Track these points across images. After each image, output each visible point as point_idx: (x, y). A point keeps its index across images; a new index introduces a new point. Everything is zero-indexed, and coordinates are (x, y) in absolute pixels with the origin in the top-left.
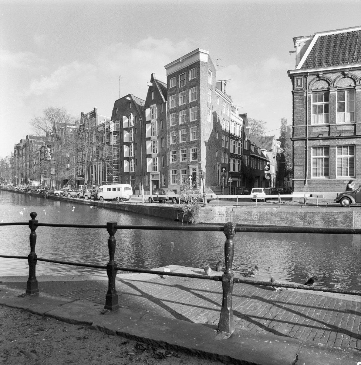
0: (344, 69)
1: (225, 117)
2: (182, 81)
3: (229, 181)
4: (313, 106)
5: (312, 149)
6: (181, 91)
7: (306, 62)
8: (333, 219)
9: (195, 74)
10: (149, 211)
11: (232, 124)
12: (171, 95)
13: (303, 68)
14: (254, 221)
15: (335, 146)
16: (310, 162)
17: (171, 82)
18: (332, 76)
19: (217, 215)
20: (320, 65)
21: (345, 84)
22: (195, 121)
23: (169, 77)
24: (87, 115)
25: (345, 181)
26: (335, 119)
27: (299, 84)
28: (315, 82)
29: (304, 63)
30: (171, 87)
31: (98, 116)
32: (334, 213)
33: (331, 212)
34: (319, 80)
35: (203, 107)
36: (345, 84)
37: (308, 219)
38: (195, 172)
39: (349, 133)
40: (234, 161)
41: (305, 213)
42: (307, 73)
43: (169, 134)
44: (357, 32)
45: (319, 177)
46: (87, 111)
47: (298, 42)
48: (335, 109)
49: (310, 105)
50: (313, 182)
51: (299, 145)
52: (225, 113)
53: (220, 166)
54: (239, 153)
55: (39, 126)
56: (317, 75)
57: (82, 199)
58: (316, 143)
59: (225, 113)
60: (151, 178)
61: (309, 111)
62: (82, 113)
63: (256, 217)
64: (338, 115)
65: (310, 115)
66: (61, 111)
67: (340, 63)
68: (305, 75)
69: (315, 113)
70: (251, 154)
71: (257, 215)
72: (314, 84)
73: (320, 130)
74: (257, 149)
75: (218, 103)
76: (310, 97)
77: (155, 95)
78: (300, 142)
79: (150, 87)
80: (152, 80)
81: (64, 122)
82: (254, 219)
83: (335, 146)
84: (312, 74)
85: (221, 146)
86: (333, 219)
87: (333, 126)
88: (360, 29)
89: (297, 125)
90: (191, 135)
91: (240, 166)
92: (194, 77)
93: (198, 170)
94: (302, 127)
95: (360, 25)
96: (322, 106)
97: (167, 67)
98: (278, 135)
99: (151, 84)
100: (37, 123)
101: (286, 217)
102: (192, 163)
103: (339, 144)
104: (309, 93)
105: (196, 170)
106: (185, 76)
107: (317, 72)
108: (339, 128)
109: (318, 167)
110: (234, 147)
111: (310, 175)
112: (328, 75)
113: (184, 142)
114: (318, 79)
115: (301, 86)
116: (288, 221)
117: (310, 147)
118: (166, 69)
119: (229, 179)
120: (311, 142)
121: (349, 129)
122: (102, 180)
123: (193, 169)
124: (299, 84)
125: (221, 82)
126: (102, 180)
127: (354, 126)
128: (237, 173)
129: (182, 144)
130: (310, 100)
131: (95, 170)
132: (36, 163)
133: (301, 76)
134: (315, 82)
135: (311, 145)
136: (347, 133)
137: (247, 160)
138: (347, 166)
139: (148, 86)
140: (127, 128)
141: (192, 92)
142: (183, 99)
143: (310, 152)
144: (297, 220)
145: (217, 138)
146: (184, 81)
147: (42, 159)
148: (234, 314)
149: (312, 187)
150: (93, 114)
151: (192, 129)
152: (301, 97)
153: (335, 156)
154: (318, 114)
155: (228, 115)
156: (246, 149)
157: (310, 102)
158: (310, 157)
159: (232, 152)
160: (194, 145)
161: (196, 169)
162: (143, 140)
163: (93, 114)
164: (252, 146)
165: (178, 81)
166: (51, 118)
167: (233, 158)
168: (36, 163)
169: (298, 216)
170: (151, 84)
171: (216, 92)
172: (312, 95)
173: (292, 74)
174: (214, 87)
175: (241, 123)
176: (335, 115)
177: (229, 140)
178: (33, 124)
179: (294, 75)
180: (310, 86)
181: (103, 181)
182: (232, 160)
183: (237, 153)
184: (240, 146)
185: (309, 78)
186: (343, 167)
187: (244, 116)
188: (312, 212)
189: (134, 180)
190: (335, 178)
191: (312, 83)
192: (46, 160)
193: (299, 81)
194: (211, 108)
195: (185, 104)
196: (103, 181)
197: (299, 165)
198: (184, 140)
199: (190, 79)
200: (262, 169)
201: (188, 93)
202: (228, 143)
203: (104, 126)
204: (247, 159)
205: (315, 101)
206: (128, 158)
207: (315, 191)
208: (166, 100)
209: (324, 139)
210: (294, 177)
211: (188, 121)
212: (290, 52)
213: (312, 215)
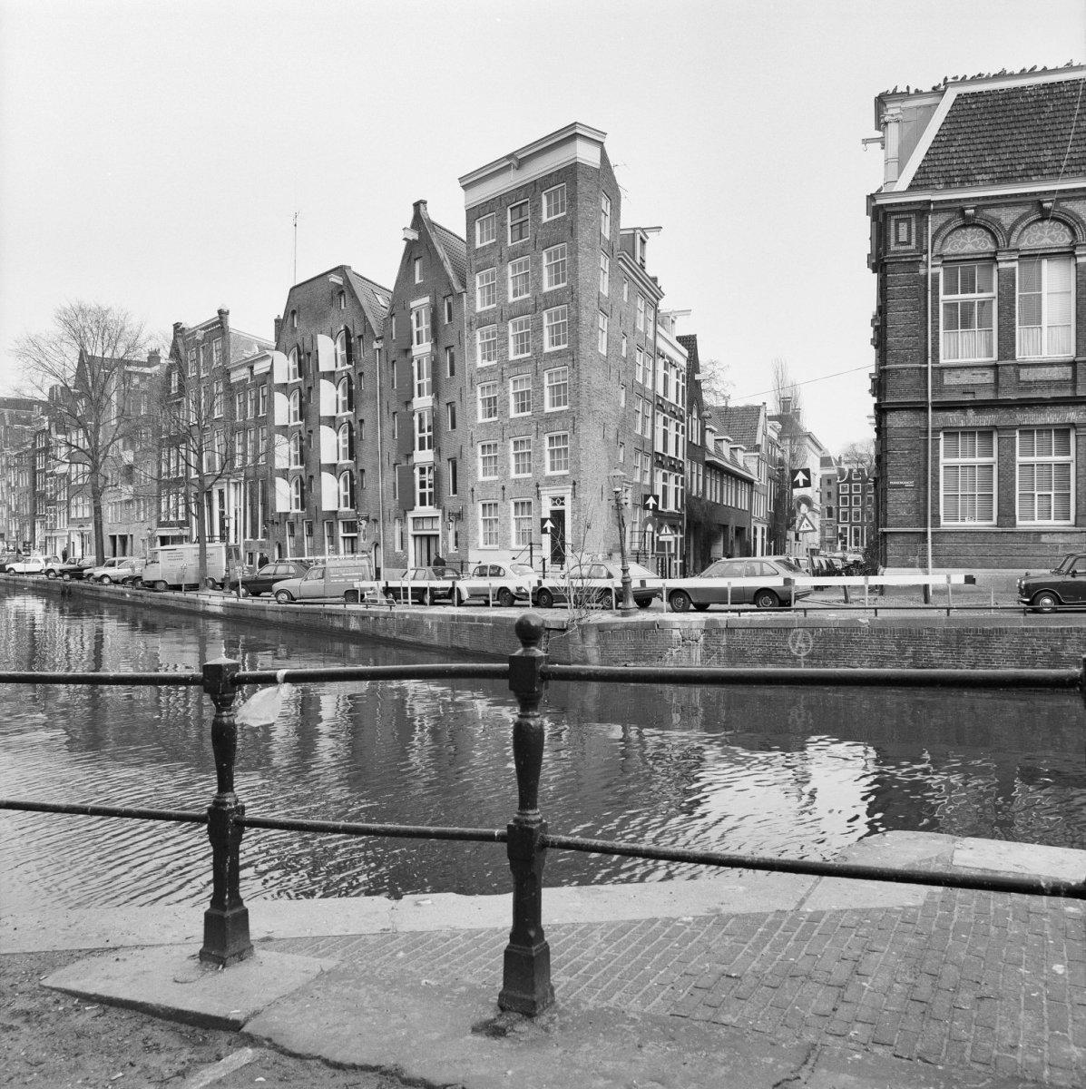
0: (1041, 193)
1: (642, 342)
2: (520, 228)
3: (661, 539)
4: (946, 305)
5: (942, 435)
6: (515, 254)
7: (921, 170)
8: (1049, 650)
9: (563, 203)
10: (435, 628)
11: (660, 363)
12: (479, 269)
13: (912, 188)
14: (795, 658)
15: (1013, 428)
16: (936, 476)
17: (482, 230)
18: (1007, 217)
19: (674, 642)
20: (967, 180)
21: (1043, 242)
22: (560, 351)
23: (473, 214)
24: (194, 333)
25: (1043, 536)
26: (1014, 346)
27: (903, 238)
28: (953, 231)
29: (917, 174)
30: (478, 245)
31: (232, 336)
32: (1050, 630)
33: (1041, 630)
34: (964, 226)
35: (587, 308)
36: (1043, 242)
37: (969, 651)
38: (559, 507)
39: (1057, 388)
40: (665, 478)
41: (958, 631)
42: (929, 202)
43: (473, 389)
44: (1076, 82)
45: (963, 523)
46: (197, 316)
47: (893, 109)
48: (1014, 316)
49: (936, 301)
50: (947, 539)
51: (901, 424)
52: (642, 329)
53: (630, 491)
54: (677, 454)
55: (39, 362)
56: (957, 208)
57: (96, 585)
58: (954, 418)
59: (642, 329)
60: (411, 531)
61: (932, 322)
62: (176, 326)
63: (803, 645)
64: (417, 452)
65: (938, 334)
66: (109, 317)
67: (1025, 177)
68: (922, 210)
69: (951, 325)
70: (708, 459)
71: (805, 641)
72: (948, 239)
73: (965, 378)
74: (719, 444)
75: (625, 299)
76: (936, 278)
77: (423, 270)
78: (906, 415)
79: (411, 245)
80: (419, 221)
81: (121, 352)
82: (794, 652)
83: (1013, 428)
84: (943, 207)
85: (630, 431)
86: (1049, 650)
87: (1006, 368)
88: (1082, 74)
89: (896, 363)
90: (547, 392)
91: (679, 492)
92: (556, 213)
93: (568, 501)
94: (912, 368)
95: (1084, 63)
96: (973, 304)
97: (469, 183)
98: (773, 408)
99: (414, 236)
100: (32, 351)
101: (898, 645)
102: (551, 481)
103: (1026, 423)
104: (933, 266)
105: (563, 504)
106: (528, 210)
107: (959, 200)
108: (1025, 375)
109: (960, 493)
110: (665, 432)
111: (936, 517)
112: (993, 212)
113: (490, 420)
114: (960, 222)
115: (909, 244)
116: (906, 658)
117: (936, 431)
118: (465, 187)
119: (663, 532)
120: (941, 414)
121: (1056, 378)
122: (245, 537)
123: (554, 499)
124: (903, 238)
125: (632, 232)
126: (245, 537)
127: (1069, 369)
128: (670, 513)
129: (550, 418)
130: (935, 287)
131: (222, 505)
132: (17, 483)
133: (909, 212)
134: (953, 231)
135: (940, 424)
136: (1049, 388)
137: (698, 475)
138: (1051, 490)
139: (405, 239)
140: (332, 373)
141: (514, 271)
142: (489, 293)
143: (936, 447)
144: (934, 654)
145: (623, 404)
146: (524, 224)
147: (40, 471)
148: (307, 768)
149: (942, 552)
150: (219, 326)
151: (550, 375)
152: (908, 278)
153: (1014, 460)
154: (960, 330)
155: (650, 336)
156: (695, 441)
157: (936, 293)
158: (936, 460)
159: (659, 449)
160: (557, 424)
161: (563, 499)
162: (385, 411)
163: (219, 326)
164: (708, 432)
165: (504, 225)
166: (79, 336)
167: (663, 468)
168: (17, 483)
169: (938, 643)
170: (414, 236)
171: (620, 262)
172: (941, 271)
173: (881, 206)
174: (617, 246)
175: (682, 362)
176: (1014, 334)
177: (653, 412)
178: (22, 354)
179: (887, 210)
180: (938, 242)
181: (248, 539)
182: (659, 476)
183: (671, 453)
184: (680, 433)
185: (933, 223)
186: (1036, 493)
187: (689, 342)
188: (983, 631)
189: (355, 535)
190: (1014, 524)
191: (943, 234)
192: (52, 474)
193: (903, 227)
194: (608, 312)
195: (561, 285)
196: (248, 539)
197: (903, 486)
198: (522, 408)
199: (545, 219)
200: (718, 501)
201: (538, 262)
202: (650, 421)
203: (252, 368)
204: (694, 471)
205: (951, 289)
206: (335, 465)
207: (953, 567)
208: (464, 286)
209: (980, 406)
210: (890, 521)
211: (538, 352)
212: (866, 141)
213: (980, 638)
